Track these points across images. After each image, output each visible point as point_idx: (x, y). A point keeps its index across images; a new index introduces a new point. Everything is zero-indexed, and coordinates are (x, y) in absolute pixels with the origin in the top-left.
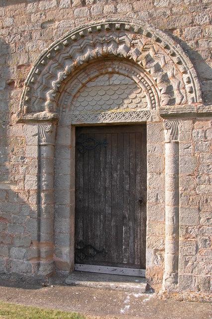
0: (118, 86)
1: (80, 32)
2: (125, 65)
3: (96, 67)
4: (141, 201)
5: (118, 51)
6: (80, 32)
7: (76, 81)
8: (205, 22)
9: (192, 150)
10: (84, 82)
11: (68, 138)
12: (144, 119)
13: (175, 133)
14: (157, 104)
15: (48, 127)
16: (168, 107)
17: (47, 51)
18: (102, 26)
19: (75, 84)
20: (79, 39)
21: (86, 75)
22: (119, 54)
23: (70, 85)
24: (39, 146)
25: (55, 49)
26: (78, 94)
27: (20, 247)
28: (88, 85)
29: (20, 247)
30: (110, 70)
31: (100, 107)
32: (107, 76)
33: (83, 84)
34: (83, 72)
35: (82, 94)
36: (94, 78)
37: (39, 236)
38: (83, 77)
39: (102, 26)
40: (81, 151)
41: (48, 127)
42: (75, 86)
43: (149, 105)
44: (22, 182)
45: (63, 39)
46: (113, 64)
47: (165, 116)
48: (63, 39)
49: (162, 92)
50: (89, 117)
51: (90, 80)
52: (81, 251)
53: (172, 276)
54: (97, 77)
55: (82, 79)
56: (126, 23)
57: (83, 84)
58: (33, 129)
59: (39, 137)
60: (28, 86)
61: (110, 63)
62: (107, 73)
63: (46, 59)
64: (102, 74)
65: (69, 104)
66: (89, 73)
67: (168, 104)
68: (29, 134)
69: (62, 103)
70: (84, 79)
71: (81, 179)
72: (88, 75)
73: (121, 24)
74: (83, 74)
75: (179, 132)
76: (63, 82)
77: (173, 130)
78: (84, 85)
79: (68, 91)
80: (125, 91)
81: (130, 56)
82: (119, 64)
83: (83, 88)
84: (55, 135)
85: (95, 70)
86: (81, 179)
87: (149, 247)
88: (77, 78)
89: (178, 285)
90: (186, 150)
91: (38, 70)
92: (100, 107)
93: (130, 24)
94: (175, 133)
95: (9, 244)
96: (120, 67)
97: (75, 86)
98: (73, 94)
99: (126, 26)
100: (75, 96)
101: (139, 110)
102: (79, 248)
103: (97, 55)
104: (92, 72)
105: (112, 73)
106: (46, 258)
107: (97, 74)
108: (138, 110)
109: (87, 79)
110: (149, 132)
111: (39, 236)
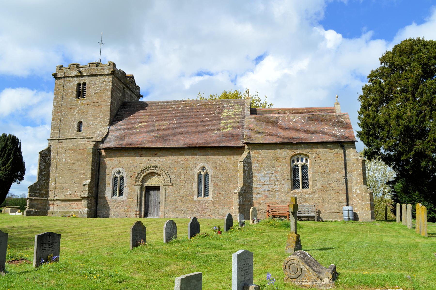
47: (164, 185)
58: (137, 186)
76: (143, 177)
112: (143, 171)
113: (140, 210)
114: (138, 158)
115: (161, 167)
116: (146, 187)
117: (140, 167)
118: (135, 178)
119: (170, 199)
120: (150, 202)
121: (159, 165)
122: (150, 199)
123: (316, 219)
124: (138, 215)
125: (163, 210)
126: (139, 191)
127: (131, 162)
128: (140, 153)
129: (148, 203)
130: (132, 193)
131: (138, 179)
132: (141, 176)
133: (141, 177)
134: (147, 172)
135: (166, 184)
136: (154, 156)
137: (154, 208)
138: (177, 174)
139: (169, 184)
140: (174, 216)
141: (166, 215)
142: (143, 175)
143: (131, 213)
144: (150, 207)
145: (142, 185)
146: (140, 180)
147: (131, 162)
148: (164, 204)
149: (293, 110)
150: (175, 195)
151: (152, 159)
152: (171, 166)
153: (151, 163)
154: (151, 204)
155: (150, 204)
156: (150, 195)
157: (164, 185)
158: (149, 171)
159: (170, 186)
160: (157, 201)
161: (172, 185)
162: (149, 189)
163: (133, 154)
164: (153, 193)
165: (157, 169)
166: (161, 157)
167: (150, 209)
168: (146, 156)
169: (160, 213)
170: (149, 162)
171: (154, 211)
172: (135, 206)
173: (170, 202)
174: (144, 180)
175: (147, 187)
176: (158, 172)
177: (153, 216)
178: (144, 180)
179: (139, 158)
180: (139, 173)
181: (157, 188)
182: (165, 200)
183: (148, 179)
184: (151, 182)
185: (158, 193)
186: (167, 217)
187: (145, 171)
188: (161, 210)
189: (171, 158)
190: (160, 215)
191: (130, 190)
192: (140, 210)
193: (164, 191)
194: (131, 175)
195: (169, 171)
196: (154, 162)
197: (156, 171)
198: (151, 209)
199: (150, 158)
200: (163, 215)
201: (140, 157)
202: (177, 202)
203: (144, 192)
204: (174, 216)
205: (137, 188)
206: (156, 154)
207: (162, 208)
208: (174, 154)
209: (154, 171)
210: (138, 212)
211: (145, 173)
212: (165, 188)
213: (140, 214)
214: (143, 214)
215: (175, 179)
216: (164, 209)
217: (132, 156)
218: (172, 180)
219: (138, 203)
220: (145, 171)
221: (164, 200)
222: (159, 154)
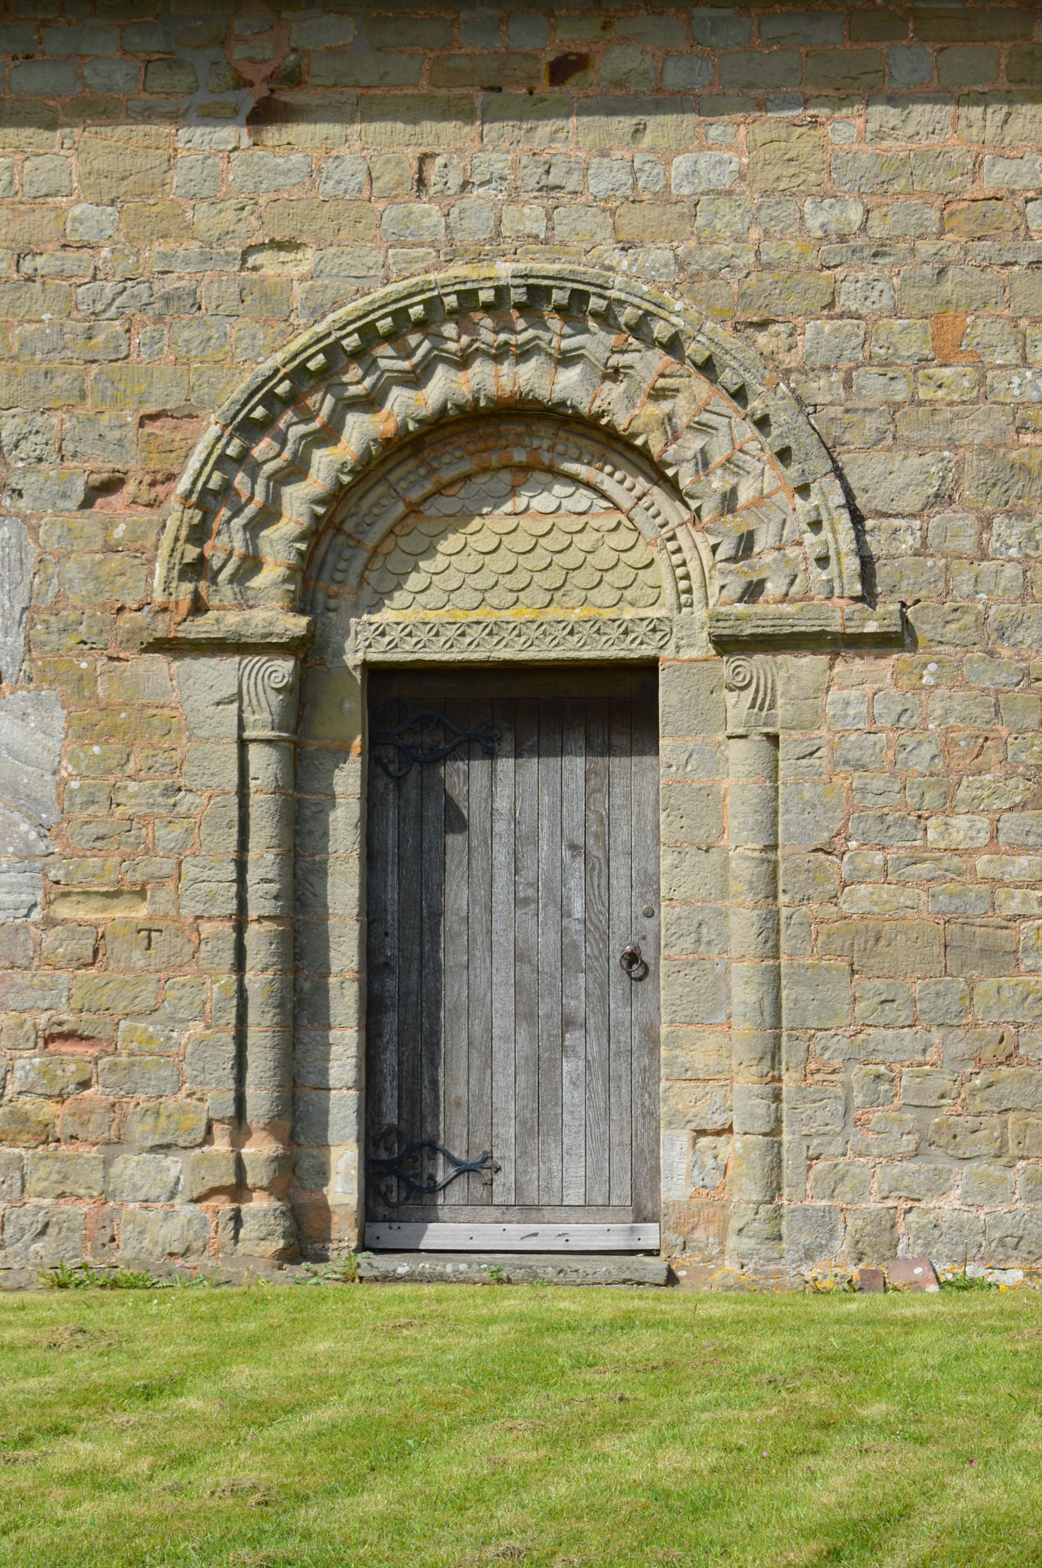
0: (584, 519)
1: (412, 306)
2: (576, 439)
3: (463, 440)
4: (632, 958)
5: (557, 387)
6: (412, 306)
7: (380, 489)
8: (876, 306)
9: (825, 762)
10: (415, 496)
11: (347, 720)
12: (647, 651)
13: (764, 700)
14: (697, 595)
15: (283, 668)
16: (740, 607)
17: (277, 371)
18: (501, 292)
19: (377, 504)
20: (410, 325)
21: (422, 471)
22: (562, 403)
23: (357, 504)
24: (243, 744)
25: (312, 365)
26: (390, 542)
27: (155, 1149)
28: (430, 510)
29: (155, 1149)
30: (519, 456)
31: (478, 597)
32: (506, 477)
33: (408, 504)
34: (413, 455)
35: (401, 542)
36: (452, 483)
37: (240, 1101)
38: (412, 478)
39: (501, 292)
40: (391, 768)
41: (283, 668)
42: (376, 511)
43: (668, 596)
44: (170, 884)
45: (341, 328)
46: (532, 435)
47: (726, 645)
48: (341, 328)
49: (722, 553)
50: (437, 634)
51: (439, 491)
52: (391, 1167)
53: (762, 1214)
54: (467, 478)
55: (404, 484)
56: (592, 289)
57: (408, 504)
58: (220, 673)
59: (241, 710)
60: (198, 505)
61: (520, 429)
62: (505, 467)
63: (270, 400)
64: (485, 470)
65: (353, 580)
66: (435, 465)
67: (740, 600)
68: (202, 700)
69: (325, 576)
70: (413, 484)
71: (392, 880)
72: (432, 471)
73: (574, 291)
74: (411, 464)
75: (780, 702)
76: (338, 497)
77: (757, 691)
78: (414, 510)
79: (349, 526)
80: (576, 538)
81: (602, 415)
82: (556, 435)
83: (410, 521)
84: (302, 701)
85: (458, 454)
86: (392, 880)
87: (670, 1123)
88: (383, 478)
89: (784, 1245)
90: (803, 762)
91: (236, 441)
92: (511, 597)
93: (608, 293)
94: (764, 700)
95: (108, 1143)
96: (560, 448)
97: (376, 511)
98: (371, 540)
99: (593, 300)
100: (375, 552)
101: (629, 613)
102: (384, 1156)
103: (477, 400)
104: (446, 459)
105: (525, 468)
106: (269, 1189)
107: (465, 467)
108: (627, 616)
109: (429, 486)
110: (668, 697)
111: (240, 1101)
112: (327, 377)
113: (298, 1118)
114: (209, 150)
115: (678, 314)
116: (376, 673)
117: (272, 304)
118: (177, 517)
119: (861, 898)
120: (452, 955)
121: (630, 275)
122: (458, 897)
123: (777, 1085)
124: (260, 1205)
125: (743, 1098)
126: (264, 764)
127: (85, 215)
128: (257, 51)
129: (429, 968)
130: (135, 795)
131: (229, 540)
132: (297, 470)
133: (298, 502)
134: (405, 406)
135: (768, 613)
136: (534, 109)
137: (542, 1071)
138: (976, 430)
139: (839, 616)
140: (948, 1205)
141: (802, 1195)
142: (326, 464)
143: (131, 1167)
144: (455, 1042)
145: (311, 653)
146: (280, 545)
147: (85, 215)
148: (744, 993)
149: (170, 650)
150: (963, 828)
151: (498, 162)
152: (859, 287)
153: (475, 226)
154: (483, 991)
155: (454, 991)
156: (455, 820)
157: (726, 645)
158: (444, 387)
159: (856, 666)
160: (597, 926)
161: (897, 640)
162: (436, 720)
163: (112, 72)
164: (514, 799)
165: (596, 342)
166: (663, 128)
167: (456, 1080)
168: (364, 107)
169: (675, 1152)
170: (428, 213)
171: (539, 1122)
172: (198, 1038)
173: (863, 947)
174: (338, 559)
175: (393, 687)
176: (619, 406)
177: (527, 1209)
178: (338, 559)
179: (230, 134)
180: (250, 429)
181: (605, 705)
182: (771, 927)
183: (416, 531)
184: (471, 592)
185: (596, 787)
186: (825, 1224)
187: (356, 381)
188: (676, 1098)
189: (850, 131)
190: (676, 1186)
191: (83, 732)
192: (298, 1118)
193: (741, 759)
194: (100, 464)
195: (821, 389)
196: (530, 217)
197: (568, 385)
198: (483, 1089)
199: (444, 135)
200: (746, 1191)
201: (264, 115)
202: (1001, 957)
203: (348, 780)
204: (948, 1205)
205: (219, 709)
206: (563, 70)
207: (706, 1062)
208: (907, 58)
209: (528, 378)
210: (260, 1150)
211: (359, 431)
212: (763, 704)
213: (297, 1176)
214: (343, 1186)
215: (958, 527)
216: (747, 1080)
217: (96, 109)
218: (895, 542)
219: (256, 981)
220: (387, 358)
221: (743, 923)
222: (617, 60)
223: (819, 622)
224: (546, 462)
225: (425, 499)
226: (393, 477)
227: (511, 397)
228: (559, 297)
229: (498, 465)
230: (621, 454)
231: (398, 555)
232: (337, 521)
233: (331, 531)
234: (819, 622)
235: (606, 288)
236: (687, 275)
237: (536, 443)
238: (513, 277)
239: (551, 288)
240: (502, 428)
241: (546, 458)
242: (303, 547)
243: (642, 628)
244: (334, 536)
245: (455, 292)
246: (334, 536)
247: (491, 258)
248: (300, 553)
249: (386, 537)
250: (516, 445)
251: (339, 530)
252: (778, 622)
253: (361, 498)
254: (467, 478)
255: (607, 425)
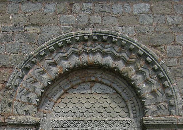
7: (58, 87)
10: (66, 88)
21: (68, 82)
22: (105, 65)
23: (51, 90)
30: (93, 79)
32: (89, 84)
36: (76, 85)
55: (64, 85)
61: (93, 72)
62: (89, 82)
64: (84, 82)
74: (65, 80)
101: (120, 119)
104: (74, 79)
107: (79, 81)
165: (161, 98)
223: (171, 121)
224: (100, 80)
225: (69, 89)
226: (61, 84)
227: (91, 63)
228: (161, 75)
229: (87, 81)
230: (119, 79)
231: (61, 103)
232: (46, 94)
233: (45, 97)
234: (171, 121)
235: (117, 36)
236: (140, 33)
237: (98, 75)
238: (93, 33)
239: (162, 71)
240: (89, 72)
241: (100, 79)
242: (67, 70)
243: (124, 122)
244: (46, 98)
245: (69, 39)
246: (46, 98)
247: (88, 28)
248: (66, 71)
249: (58, 99)
250: (92, 76)
251: (47, 97)
252: (161, 121)
253: (53, 89)
254: (79, 84)
255: (116, 71)
